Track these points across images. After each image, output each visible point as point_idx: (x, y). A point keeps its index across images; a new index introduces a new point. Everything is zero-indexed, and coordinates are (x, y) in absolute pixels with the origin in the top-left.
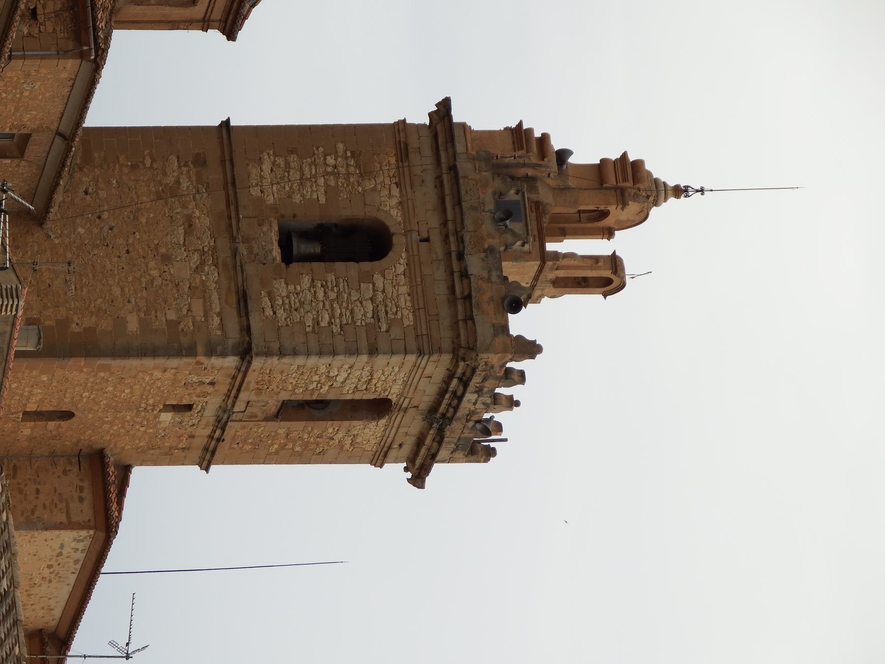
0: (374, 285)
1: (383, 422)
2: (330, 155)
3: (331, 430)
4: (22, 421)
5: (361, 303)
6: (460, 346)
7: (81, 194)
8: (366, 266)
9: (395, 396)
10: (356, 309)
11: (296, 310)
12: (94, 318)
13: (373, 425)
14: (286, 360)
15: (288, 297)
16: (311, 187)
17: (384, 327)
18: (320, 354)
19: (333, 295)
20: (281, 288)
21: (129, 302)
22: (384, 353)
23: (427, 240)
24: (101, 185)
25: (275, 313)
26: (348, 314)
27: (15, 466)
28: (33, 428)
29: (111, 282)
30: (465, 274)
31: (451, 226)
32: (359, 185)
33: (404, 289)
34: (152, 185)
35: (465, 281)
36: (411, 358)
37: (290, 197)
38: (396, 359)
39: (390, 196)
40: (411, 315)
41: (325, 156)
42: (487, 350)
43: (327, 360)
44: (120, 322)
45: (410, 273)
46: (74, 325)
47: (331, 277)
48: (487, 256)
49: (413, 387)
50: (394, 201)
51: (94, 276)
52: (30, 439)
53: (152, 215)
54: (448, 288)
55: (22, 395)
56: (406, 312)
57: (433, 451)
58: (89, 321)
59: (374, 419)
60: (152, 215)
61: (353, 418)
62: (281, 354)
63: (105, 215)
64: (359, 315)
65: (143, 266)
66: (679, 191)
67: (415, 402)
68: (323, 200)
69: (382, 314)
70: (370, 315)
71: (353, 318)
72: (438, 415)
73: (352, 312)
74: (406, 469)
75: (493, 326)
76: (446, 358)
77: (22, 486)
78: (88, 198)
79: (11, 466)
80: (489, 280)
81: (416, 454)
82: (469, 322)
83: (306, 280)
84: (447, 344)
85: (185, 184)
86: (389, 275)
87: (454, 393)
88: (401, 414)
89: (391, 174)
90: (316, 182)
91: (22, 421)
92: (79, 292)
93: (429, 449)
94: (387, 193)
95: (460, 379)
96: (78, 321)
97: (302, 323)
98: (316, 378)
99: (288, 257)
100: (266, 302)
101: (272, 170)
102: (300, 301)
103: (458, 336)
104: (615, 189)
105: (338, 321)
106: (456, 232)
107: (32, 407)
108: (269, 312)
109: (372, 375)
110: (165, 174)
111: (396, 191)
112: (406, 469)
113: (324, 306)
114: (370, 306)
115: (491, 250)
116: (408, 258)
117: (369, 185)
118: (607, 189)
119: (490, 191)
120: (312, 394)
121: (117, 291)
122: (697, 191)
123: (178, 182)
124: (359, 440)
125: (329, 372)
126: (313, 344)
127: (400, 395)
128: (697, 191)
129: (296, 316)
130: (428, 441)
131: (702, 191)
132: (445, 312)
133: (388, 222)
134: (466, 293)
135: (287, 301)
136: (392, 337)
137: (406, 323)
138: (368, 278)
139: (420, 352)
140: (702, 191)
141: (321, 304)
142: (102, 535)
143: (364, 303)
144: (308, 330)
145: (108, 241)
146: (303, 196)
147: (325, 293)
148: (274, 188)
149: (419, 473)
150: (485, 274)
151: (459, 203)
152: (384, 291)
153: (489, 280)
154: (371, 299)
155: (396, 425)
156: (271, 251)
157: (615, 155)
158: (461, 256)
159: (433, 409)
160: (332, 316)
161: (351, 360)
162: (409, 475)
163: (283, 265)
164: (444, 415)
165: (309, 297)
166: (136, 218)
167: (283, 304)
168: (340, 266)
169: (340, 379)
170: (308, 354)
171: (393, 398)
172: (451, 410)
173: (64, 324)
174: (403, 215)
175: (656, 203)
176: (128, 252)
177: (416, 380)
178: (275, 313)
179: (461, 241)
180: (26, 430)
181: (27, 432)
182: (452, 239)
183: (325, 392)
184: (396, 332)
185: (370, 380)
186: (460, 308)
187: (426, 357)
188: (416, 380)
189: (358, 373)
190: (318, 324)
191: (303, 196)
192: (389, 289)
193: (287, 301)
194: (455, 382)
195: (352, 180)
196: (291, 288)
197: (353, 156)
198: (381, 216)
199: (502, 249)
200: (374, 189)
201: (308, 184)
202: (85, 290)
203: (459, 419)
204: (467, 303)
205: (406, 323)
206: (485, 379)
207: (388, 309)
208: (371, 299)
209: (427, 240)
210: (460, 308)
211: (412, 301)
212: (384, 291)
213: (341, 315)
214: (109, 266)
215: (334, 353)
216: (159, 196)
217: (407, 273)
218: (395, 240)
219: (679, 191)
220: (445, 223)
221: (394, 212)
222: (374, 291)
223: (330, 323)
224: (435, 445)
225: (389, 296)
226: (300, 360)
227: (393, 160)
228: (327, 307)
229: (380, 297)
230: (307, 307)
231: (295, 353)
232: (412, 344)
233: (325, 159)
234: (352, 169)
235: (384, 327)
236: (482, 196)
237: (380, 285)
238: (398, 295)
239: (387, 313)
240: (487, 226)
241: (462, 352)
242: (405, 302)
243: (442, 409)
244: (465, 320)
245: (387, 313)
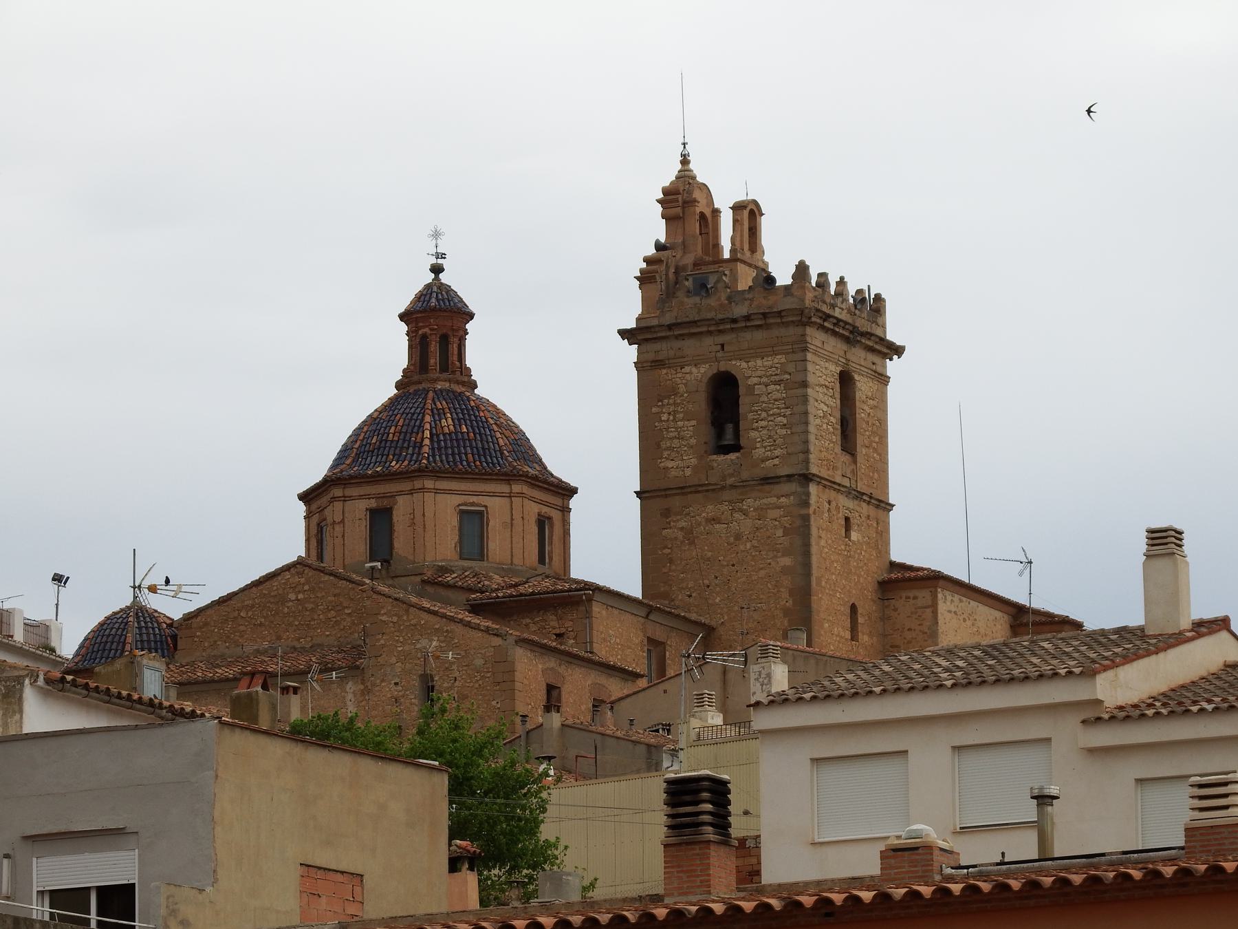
0: (756, 384)
1: (856, 377)
2: (660, 417)
3: (863, 415)
4: (858, 641)
5: (769, 394)
6: (800, 321)
7: (691, 600)
8: (742, 390)
9: (837, 368)
10: (773, 398)
11: (775, 441)
12: (782, 590)
13: (858, 384)
14: (812, 448)
15: (765, 447)
16: (685, 431)
17: (787, 376)
18: (807, 423)
19: (764, 415)
20: (759, 452)
21: (770, 564)
22: (806, 376)
23: (723, 345)
24: (684, 585)
25: (777, 457)
26: (777, 403)
27: (891, 647)
28: (863, 634)
29: (756, 577)
30: (747, 318)
31: (712, 328)
32: (682, 396)
33: (759, 362)
34: (683, 548)
35: (752, 317)
36: (809, 356)
37: (692, 447)
38: (810, 367)
39: (691, 373)
40: (777, 357)
41: (662, 421)
42: (803, 300)
43: (811, 418)
44: (785, 570)
45: (747, 357)
46: (787, 604)
47: (750, 416)
48: (734, 302)
49: (831, 355)
50: (694, 370)
51: (752, 590)
52: (871, 635)
53: (706, 548)
54: (757, 330)
55: (839, 642)
56: (776, 361)
57: (878, 340)
58: (785, 594)
59: (855, 384)
60: (706, 548)
61: (854, 399)
62: (807, 452)
63: (706, 582)
64: (778, 395)
65: (743, 554)
66: (685, 161)
67: (842, 353)
68: (694, 423)
69: (777, 378)
70: (778, 387)
71: (780, 400)
72: (851, 336)
73: (776, 400)
74: (891, 359)
75: (785, 296)
76: (809, 331)
77: (906, 641)
78: (694, 595)
79: (891, 649)
80: (752, 300)
81: (879, 352)
82: (783, 314)
83: (753, 434)
84: (799, 330)
85: (683, 524)
86: (747, 374)
87: (835, 324)
88: (850, 363)
89: (675, 372)
90: (680, 428)
91: (858, 641)
92: (763, 601)
93: (876, 343)
94: (688, 375)
95: (825, 320)
96: (785, 602)
97: (784, 437)
98: (825, 426)
99: (736, 448)
100: (769, 463)
101: (672, 460)
102: (768, 439)
103: (792, 321)
104: (683, 208)
105: (782, 411)
106: (717, 324)
107: (848, 635)
108: (776, 461)
109: (822, 385)
110: (676, 538)
111: (687, 369)
112: (891, 359)
113: (772, 421)
114: (772, 387)
115: (729, 298)
116: (736, 359)
117: (682, 388)
118: (683, 213)
119: (686, 300)
120: (837, 429)
121: (762, 573)
122: (685, 147)
123: (682, 529)
124: (870, 394)
125: (820, 417)
126: (800, 428)
127: (837, 364)
128: (685, 147)
129: (779, 441)
130: (870, 343)
131: (684, 144)
132: (776, 332)
133: (710, 374)
134: (761, 316)
135: (769, 448)
136: (794, 371)
137: (783, 360)
138: (751, 389)
139: (805, 350)
140: (684, 144)
141: (770, 423)
142: (941, 582)
143: (770, 391)
144: (789, 433)
145: (725, 580)
146: (691, 437)
147: (762, 420)
148: (685, 458)
149: (894, 350)
150: (747, 303)
151: (695, 322)
152: (760, 377)
153: (752, 300)
154: (766, 386)
155: (858, 367)
156: (732, 460)
157: (659, 208)
158: (734, 321)
159: (847, 340)
160: (779, 415)
161: (811, 400)
162: (895, 357)
163: (742, 451)
164: (851, 332)
165: (765, 432)
166: (709, 559)
167: (770, 451)
168: (742, 410)
169: (825, 408)
170: (807, 432)
171: (839, 369)
172: (847, 327)
173: (786, 612)
174: (705, 363)
175: (694, 178)
176: (733, 565)
177: (826, 353)
178: (777, 457)
179: (722, 321)
180: (864, 638)
181: (866, 638)
182: (721, 327)
183: (835, 419)
184: (791, 368)
185: (826, 386)
186: (772, 321)
187: (809, 345)
188: (826, 353)
189: (821, 395)
190: (785, 425)
191: (691, 437)
192: (759, 373)
193: (769, 448)
194: (826, 324)
195: (679, 401)
196: (758, 445)
197: (661, 401)
198: (705, 380)
199: (728, 290)
200: (685, 385)
201: (682, 433)
202: (761, 597)
203: (854, 321)
204: (769, 316)
205: (783, 360)
206: (824, 302)
207: (774, 373)
208: (766, 386)
209: (723, 345)
210: (772, 321)
211: (768, 356)
212: (760, 377)
213: (778, 408)
214: (744, 579)
215: (806, 413)
216: (692, 543)
217: (747, 360)
218: (722, 369)
219: (685, 161)
220: (710, 333)
221: (702, 370)
222: (760, 384)
223: (784, 416)
224: (873, 338)
225: (763, 373)
226: (812, 438)
227: (664, 371)
228: (772, 418)
229: (764, 380)
230: (773, 433)
231: (806, 442)
232: (799, 356)
233: (664, 421)
234: (671, 401)
235: (787, 376)
236: (690, 306)
237: (755, 380)
238: (763, 367)
239: (776, 375)
240: (712, 302)
241: (804, 319)
242: (768, 362)
243: (847, 334)
244: (782, 317)
245: (776, 375)
